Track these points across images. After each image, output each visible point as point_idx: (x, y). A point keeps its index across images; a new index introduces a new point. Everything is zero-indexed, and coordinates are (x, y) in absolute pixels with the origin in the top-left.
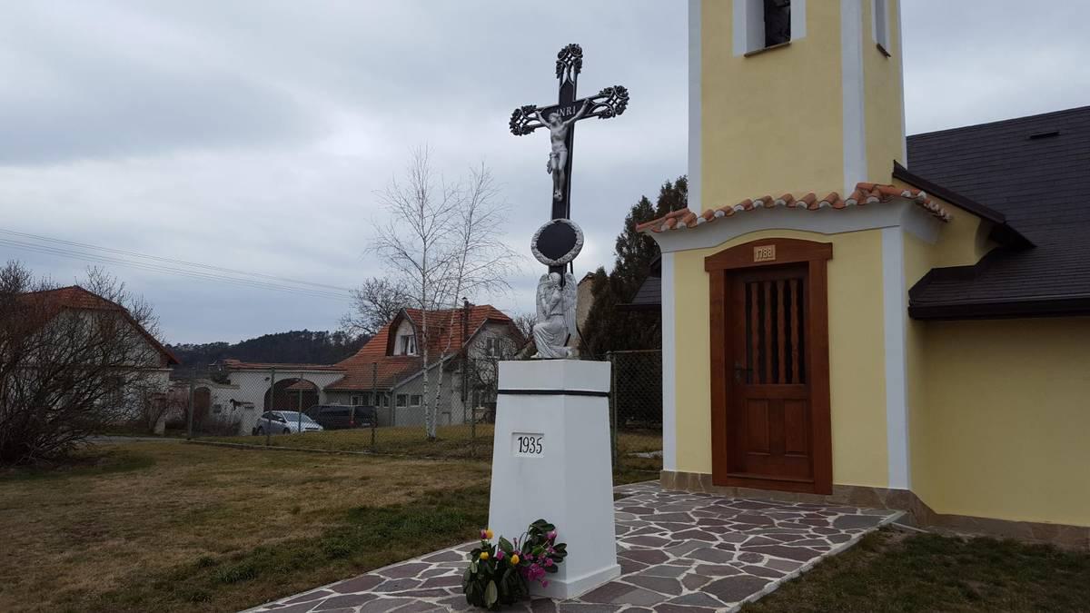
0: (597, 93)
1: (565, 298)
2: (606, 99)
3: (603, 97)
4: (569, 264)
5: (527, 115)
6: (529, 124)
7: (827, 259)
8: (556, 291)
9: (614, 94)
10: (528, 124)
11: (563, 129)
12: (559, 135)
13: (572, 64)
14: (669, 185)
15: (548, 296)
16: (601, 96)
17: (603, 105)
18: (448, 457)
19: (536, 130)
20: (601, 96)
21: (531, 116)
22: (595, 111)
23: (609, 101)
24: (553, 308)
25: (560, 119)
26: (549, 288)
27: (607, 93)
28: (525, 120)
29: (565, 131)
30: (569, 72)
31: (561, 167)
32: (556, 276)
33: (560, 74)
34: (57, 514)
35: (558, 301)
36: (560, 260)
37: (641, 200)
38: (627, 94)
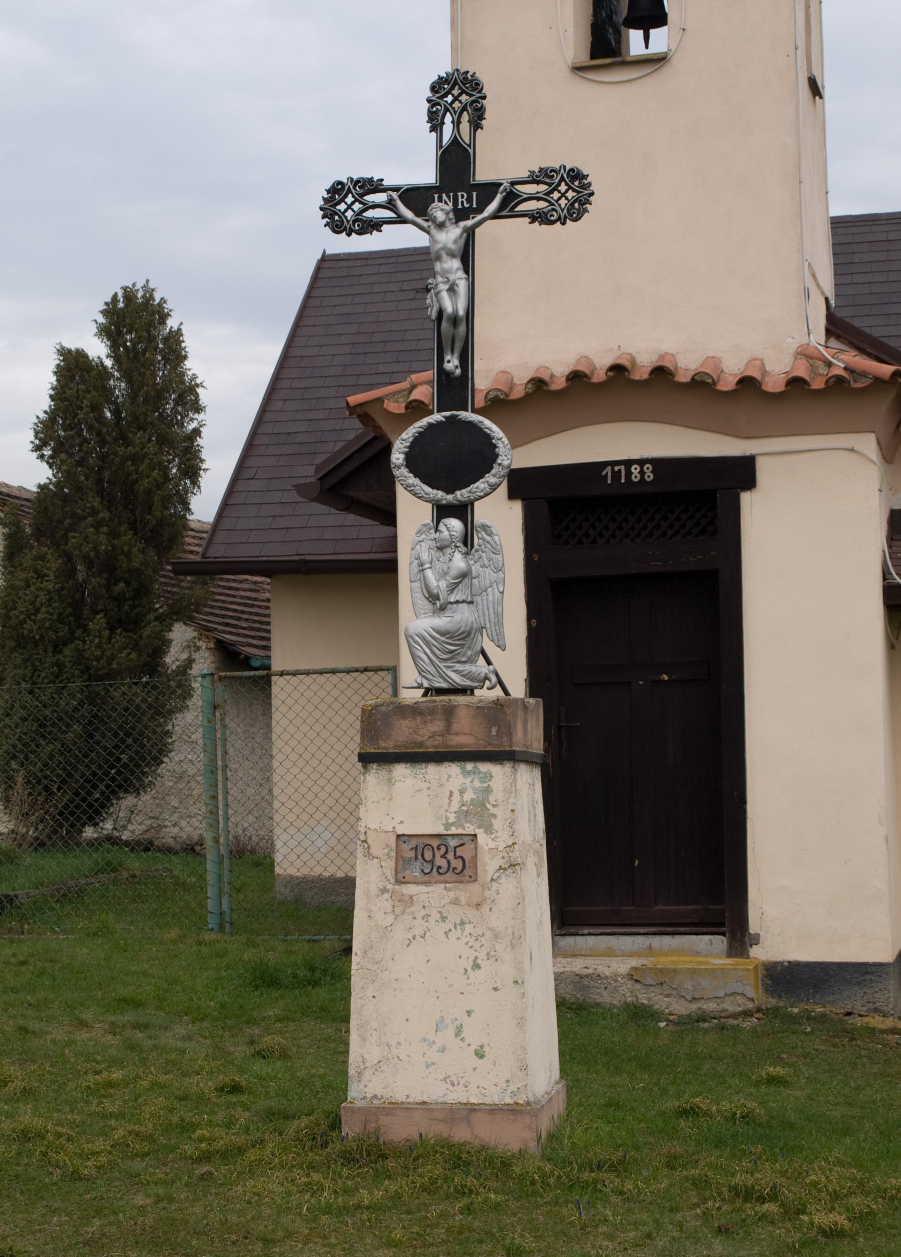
0: (525, 174)
1: (476, 569)
2: (543, 188)
3: (538, 183)
4: (469, 507)
5: (362, 196)
6: (370, 214)
7: (760, 386)
8: (458, 557)
9: (562, 179)
10: (366, 214)
11: (461, 235)
12: (453, 247)
13: (464, 109)
14: (200, 437)
15: (438, 565)
16: (533, 180)
17: (538, 199)
18: (382, 705)
19: (385, 227)
20: (533, 180)
21: (371, 198)
22: (522, 207)
23: (551, 192)
24: (452, 588)
25: (451, 216)
26: (440, 549)
27: (547, 176)
28: (357, 207)
29: (462, 242)
30: (457, 124)
31: (461, 312)
32: (455, 525)
33: (436, 124)
34: (32, 700)
35: (464, 575)
36: (462, 495)
37: (585, 173)
38: (590, 184)
